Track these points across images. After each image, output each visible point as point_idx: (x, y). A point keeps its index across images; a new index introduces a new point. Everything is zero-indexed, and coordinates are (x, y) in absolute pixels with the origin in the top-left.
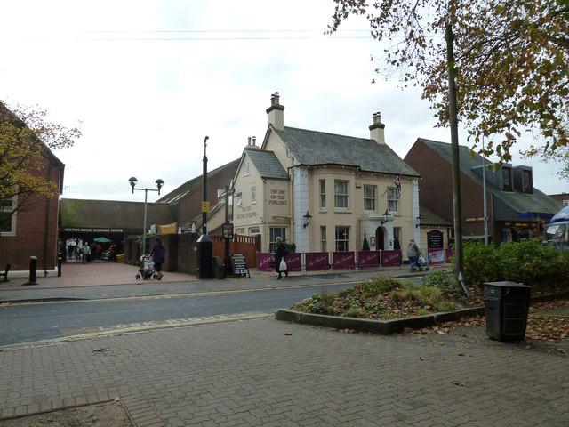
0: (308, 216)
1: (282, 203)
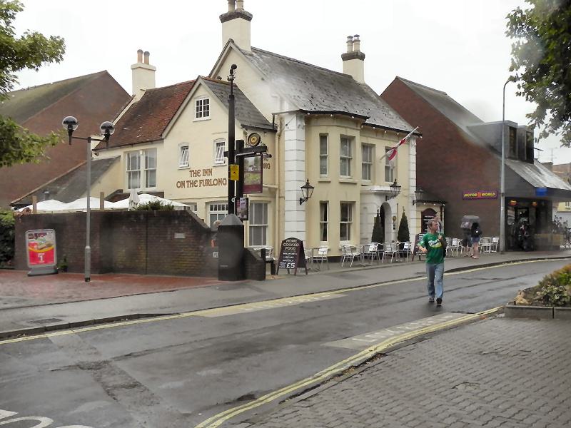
0: (308, 186)
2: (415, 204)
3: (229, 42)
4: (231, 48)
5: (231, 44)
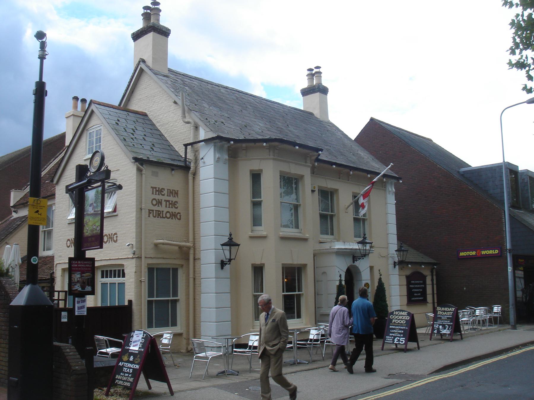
0: (231, 243)
1: (173, 216)
2: (397, 267)
3: (139, 62)
4: (142, 70)
5: (142, 65)
